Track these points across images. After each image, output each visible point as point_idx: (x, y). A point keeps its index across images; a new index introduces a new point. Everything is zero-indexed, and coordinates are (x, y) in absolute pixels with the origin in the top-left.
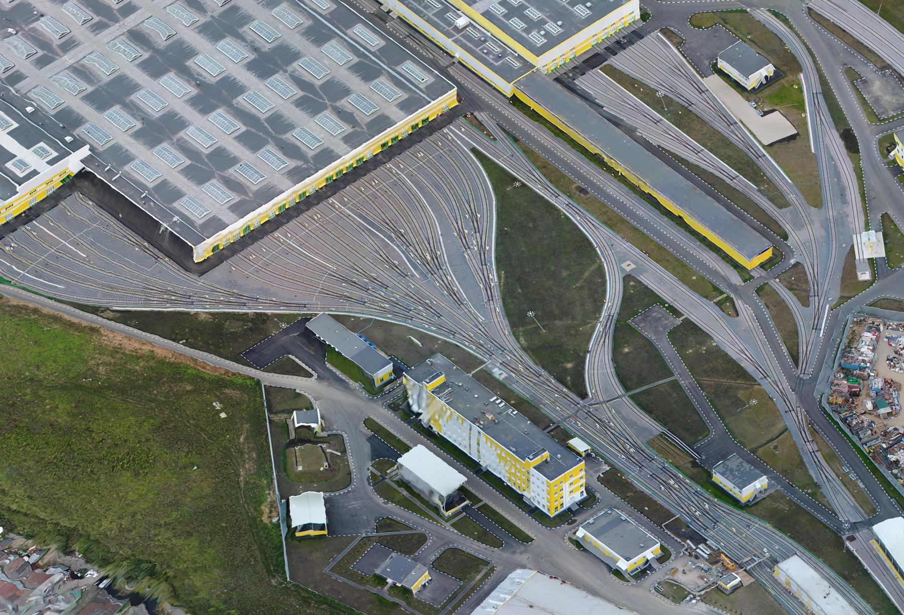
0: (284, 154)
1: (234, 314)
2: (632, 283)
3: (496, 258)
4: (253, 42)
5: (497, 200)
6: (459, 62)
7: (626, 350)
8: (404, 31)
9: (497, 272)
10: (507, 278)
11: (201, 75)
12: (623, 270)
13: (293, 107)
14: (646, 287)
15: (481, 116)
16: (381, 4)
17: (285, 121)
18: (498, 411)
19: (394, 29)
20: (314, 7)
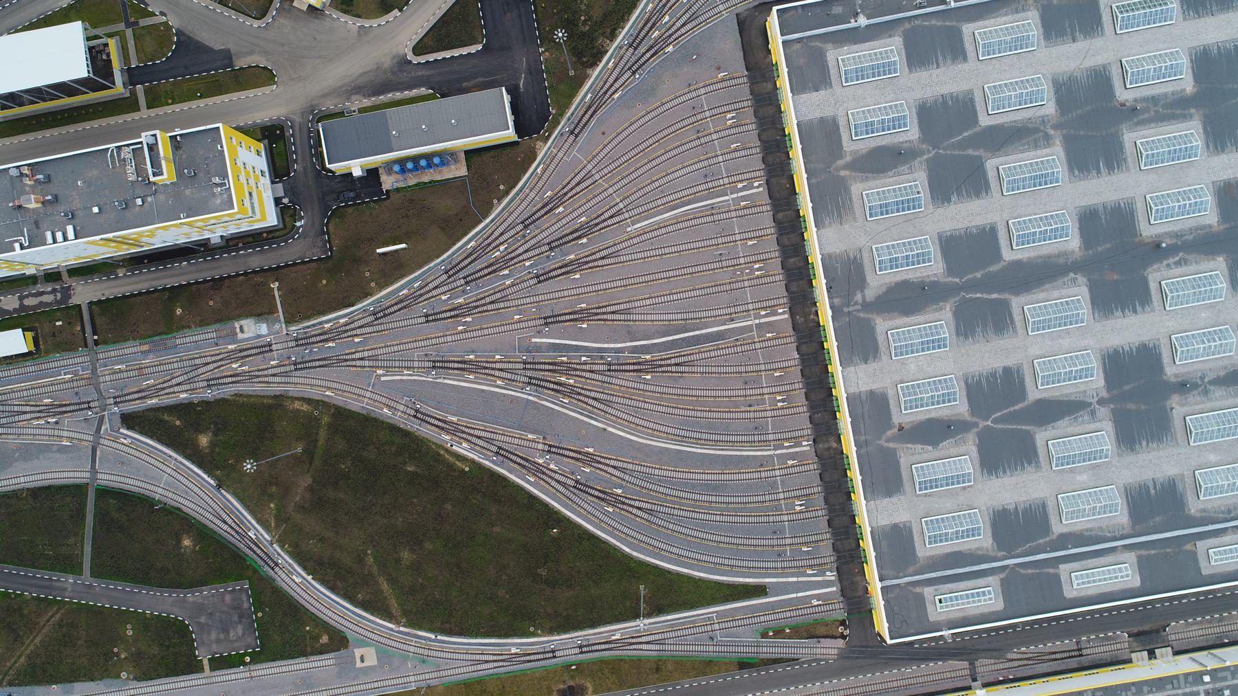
0: (905, 284)
1: (623, 19)
2: (325, 639)
3: (505, 479)
4: (1206, 393)
5: (630, 557)
6: (969, 688)
7: (187, 542)
8: (1096, 651)
9: (473, 461)
10: (451, 467)
11: (1178, 264)
12: (363, 643)
13: (1010, 362)
14: (304, 654)
15: (830, 649)
16: (1176, 653)
17: (984, 330)
18: (43, 226)
19: (1107, 638)
20: (1226, 539)
